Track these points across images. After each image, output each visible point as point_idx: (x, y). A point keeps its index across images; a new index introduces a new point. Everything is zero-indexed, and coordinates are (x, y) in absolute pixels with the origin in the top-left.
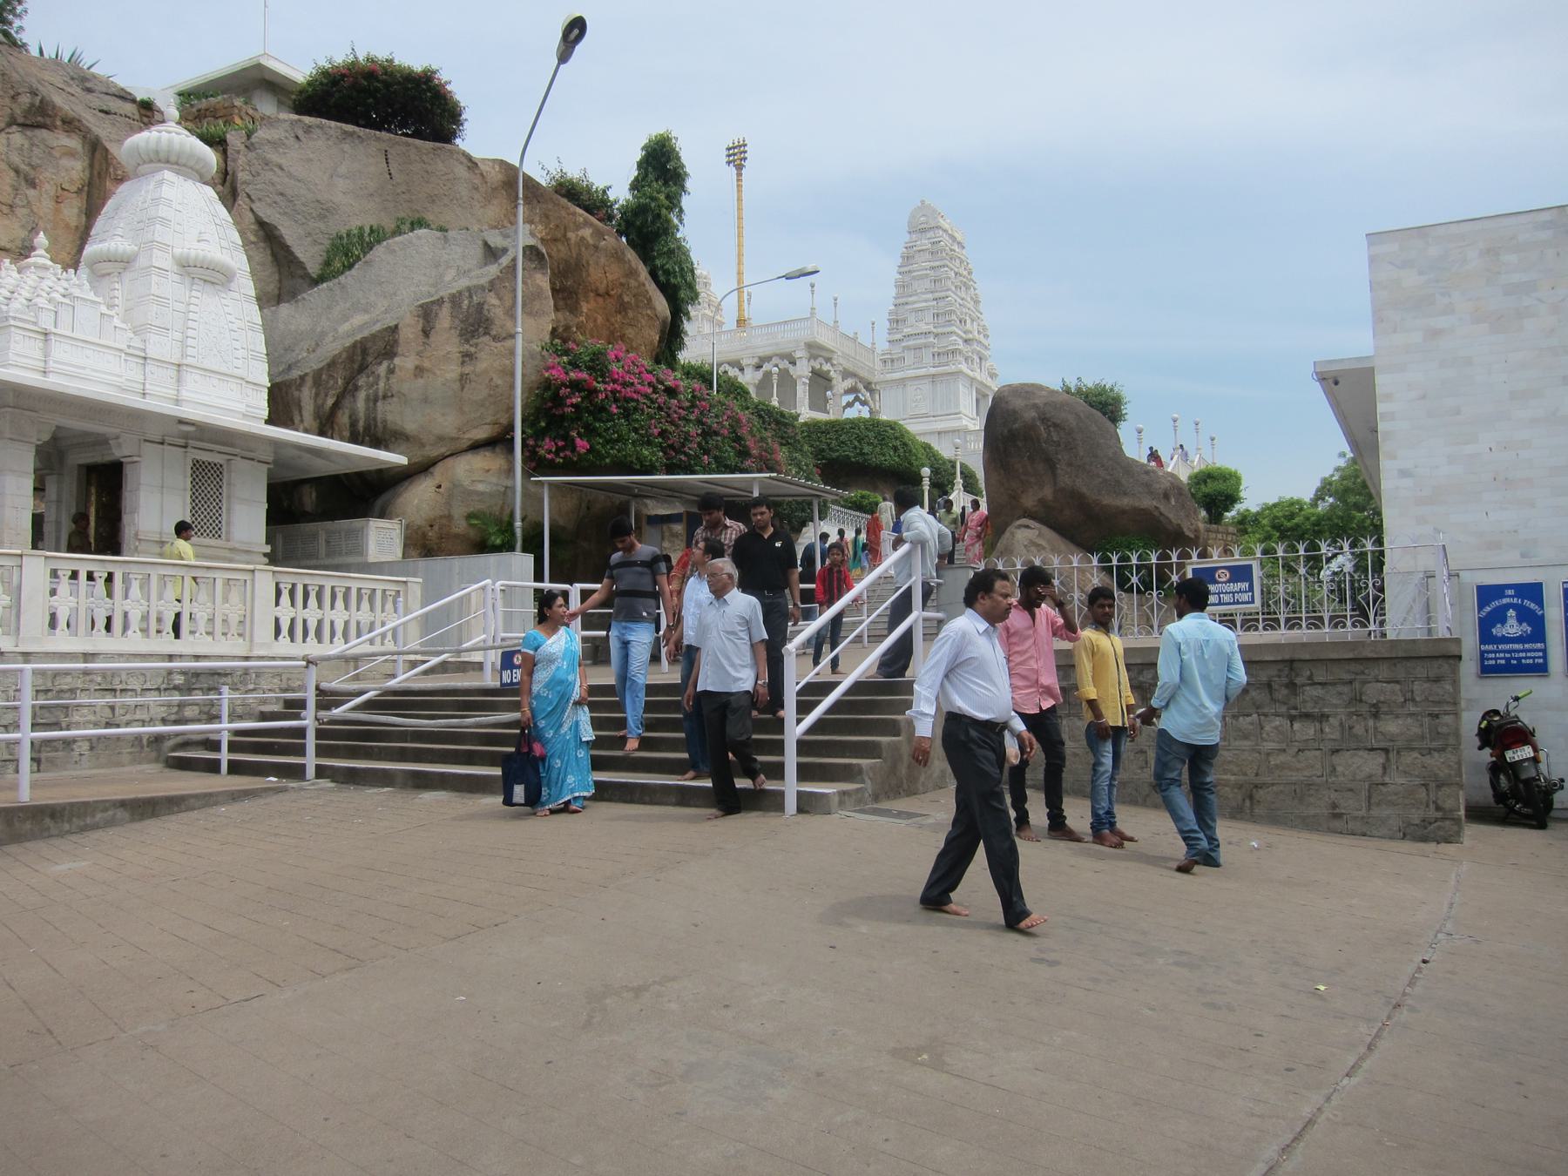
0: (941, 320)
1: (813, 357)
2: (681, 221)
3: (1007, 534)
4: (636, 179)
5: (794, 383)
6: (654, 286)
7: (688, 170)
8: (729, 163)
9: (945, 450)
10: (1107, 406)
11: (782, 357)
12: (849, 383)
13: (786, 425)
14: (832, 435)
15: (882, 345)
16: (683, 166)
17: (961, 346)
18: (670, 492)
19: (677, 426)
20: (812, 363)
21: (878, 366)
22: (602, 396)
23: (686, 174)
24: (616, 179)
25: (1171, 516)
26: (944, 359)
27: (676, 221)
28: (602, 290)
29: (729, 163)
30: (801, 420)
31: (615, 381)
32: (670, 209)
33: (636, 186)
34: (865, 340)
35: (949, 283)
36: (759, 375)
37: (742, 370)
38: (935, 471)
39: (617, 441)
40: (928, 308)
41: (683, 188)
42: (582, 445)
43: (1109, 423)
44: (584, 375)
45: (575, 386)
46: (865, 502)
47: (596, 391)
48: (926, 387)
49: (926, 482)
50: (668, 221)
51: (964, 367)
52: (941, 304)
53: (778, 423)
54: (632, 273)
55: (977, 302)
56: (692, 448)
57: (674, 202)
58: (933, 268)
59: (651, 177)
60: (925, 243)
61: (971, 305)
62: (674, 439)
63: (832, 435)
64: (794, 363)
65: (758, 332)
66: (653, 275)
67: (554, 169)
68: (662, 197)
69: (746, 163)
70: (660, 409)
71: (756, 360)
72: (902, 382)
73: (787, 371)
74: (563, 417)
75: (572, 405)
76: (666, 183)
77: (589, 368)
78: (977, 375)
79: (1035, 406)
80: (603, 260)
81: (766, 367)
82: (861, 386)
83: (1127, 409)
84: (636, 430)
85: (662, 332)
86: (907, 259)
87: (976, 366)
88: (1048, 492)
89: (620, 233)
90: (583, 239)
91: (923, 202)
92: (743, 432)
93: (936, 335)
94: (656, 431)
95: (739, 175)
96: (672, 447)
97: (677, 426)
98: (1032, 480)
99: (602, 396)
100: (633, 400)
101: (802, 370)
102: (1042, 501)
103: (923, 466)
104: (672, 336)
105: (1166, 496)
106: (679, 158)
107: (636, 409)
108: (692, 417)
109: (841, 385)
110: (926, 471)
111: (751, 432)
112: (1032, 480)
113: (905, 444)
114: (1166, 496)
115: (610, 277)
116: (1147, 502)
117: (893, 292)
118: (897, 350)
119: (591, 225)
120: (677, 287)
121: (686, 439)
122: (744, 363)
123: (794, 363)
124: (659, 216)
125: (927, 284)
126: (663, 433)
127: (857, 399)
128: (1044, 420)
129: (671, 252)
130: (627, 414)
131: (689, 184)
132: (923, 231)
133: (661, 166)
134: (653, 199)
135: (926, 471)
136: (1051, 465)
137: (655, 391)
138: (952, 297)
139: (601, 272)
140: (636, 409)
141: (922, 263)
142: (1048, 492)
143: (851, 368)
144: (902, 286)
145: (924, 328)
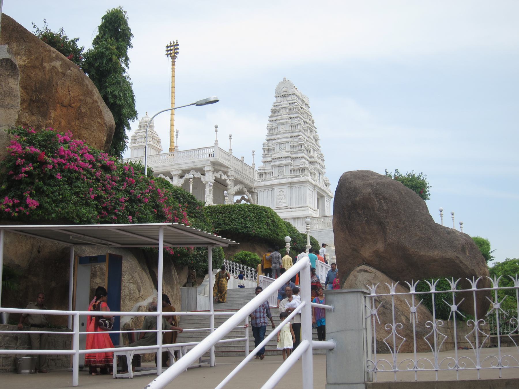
0: (296, 150)
1: (216, 171)
2: (127, 65)
3: (351, 277)
4: (98, 37)
5: (204, 186)
6: (104, 103)
7: (132, 32)
8: (167, 55)
9: (300, 228)
10: (417, 187)
11: (197, 170)
12: (238, 188)
13: (195, 204)
14: (226, 215)
15: (259, 165)
16: (129, 29)
17: (308, 165)
18: (102, 238)
19: (110, 194)
20: (215, 174)
21: (257, 177)
22: (50, 167)
23: (132, 35)
24: (85, 37)
25: (467, 263)
26: (297, 173)
27: (123, 65)
28: (66, 102)
29: (167, 55)
30: (206, 205)
31: (61, 157)
32: (119, 56)
33: (96, 42)
34: (248, 161)
35: (300, 127)
36: (182, 181)
37: (171, 178)
38: (293, 241)
39: (61, 201)
40: (287, 142)
41: (129, 44)
42: (33, 203)
43: (421, 199)
44: (37, 150)
45: (30, 158)
46: (248, 259)
47: (46, 163)
48: (286, 190)
49: (288, 245)
50: (117, 64)
51: (309, 178)
52: (296, 140)
53: (189, 203)
54: (89, 93)
55: (317, 140)
56: (121, 210)
57: (122, 52)
58: (290, 118)
59: (107, 35)
60: (285, 102)
61: (314, 141)
62: (107, 203)
63: (226, 215)
64: (204, 175)
65: (182, 154)
66: (105, 98)
67: (41, 27)
68: (114, 48)
69: (178, 55)
70: (98, 180)
71: (180, 172)
72: (271, 187)
73: (199, 179)
74: (20, 182)
75: (26, 172)
76: (117, 39)
77: (41, 146)
78: (317, 183)
79: (370, 185)
80: (68, 83)
81: (187, 176)
82: (245, 190)
83: (431, 191)
84: (77, 194)
85: (109, 136)
86: (275, 112)
87: (317, 178)
88: (380, 246)
89: (85, 71)
90: (54, 68)
91: (284, 79)
92: (160, 202)
93: (293, 159)
94: (93, 196)
95: (173, 62)
96: (105, 208)
97: (110, 194)
98: (369, 237)
99: (50, 167)
100: (76, 172)
101: (209, 178)
102: (376, 253)
103: (285, 236)
104: (116, 141)
105: (463, 250)
106: (126, 24)
107: (77, 179)
108: (121, 188)
109: (233, 189)
110: (288, 238)
111: (167, 203)
112: (369, 237)
113: (274, 221)
114: (463, 250)
115: (72, 95)
116: (451, 254)
117: (266, 132)
118: (268, 167)
119: (61, 59)
120: (122, 105)
121: (116, 203)
122: (173, 173)
123: (204, 175)
124: (111, 60)
125: (287, 128)
126: (98, 198)
127: (243, 198)
128: (377, 194)
129: (118, 83)
130: (70, 182)
131: (133, 41)
132: (284, 96)
133: (115, 29)
134: (107, 49)
135: (288, 238)
136: (382, 227)
137: (94, 166)
138: (302, 136)
139: (65, 91)
140: (77, 179)
141: (284, 114)
142: (380, 246)
143: (239, 178)
144: (271, 129)
145: (284, 154)
